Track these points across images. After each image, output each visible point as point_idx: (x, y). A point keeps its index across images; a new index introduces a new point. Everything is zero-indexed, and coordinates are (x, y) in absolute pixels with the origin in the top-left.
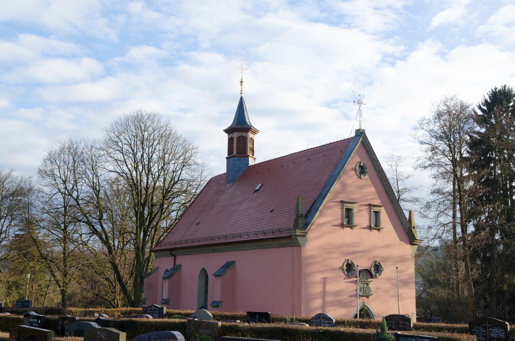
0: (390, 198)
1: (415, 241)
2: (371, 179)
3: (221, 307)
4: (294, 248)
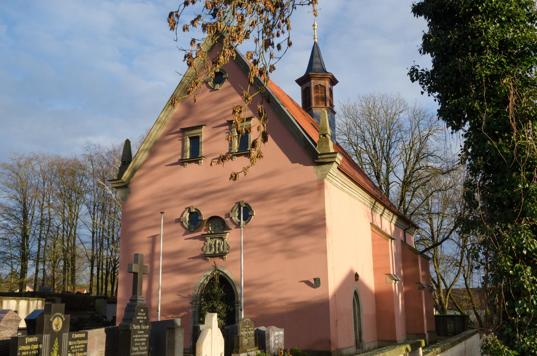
1: (319, 157)
2: (234, 85)
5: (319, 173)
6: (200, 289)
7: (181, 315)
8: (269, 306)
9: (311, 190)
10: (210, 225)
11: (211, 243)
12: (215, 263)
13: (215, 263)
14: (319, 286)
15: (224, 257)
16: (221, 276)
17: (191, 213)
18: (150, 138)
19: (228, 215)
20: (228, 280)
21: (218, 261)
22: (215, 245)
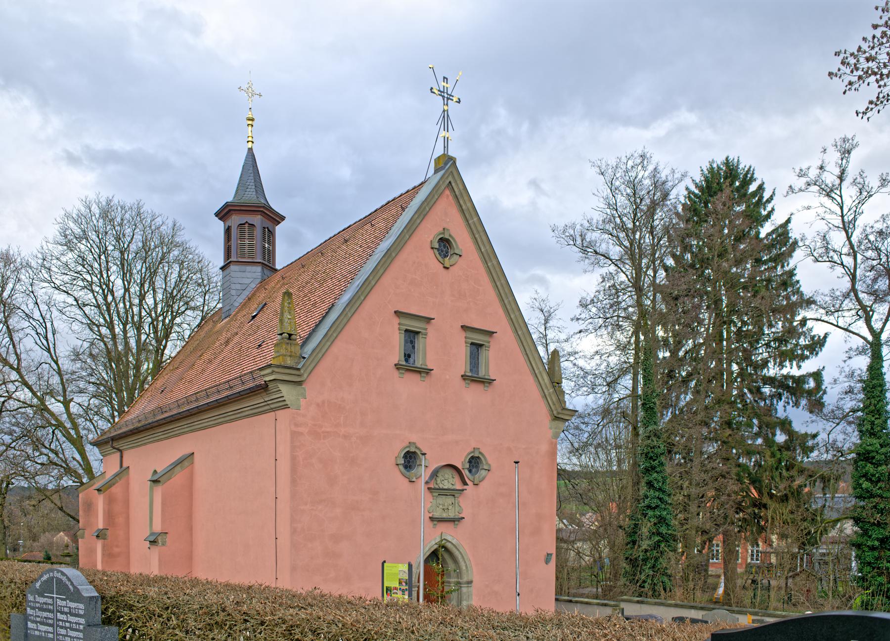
3: (163, 545)
4: (276, 412)
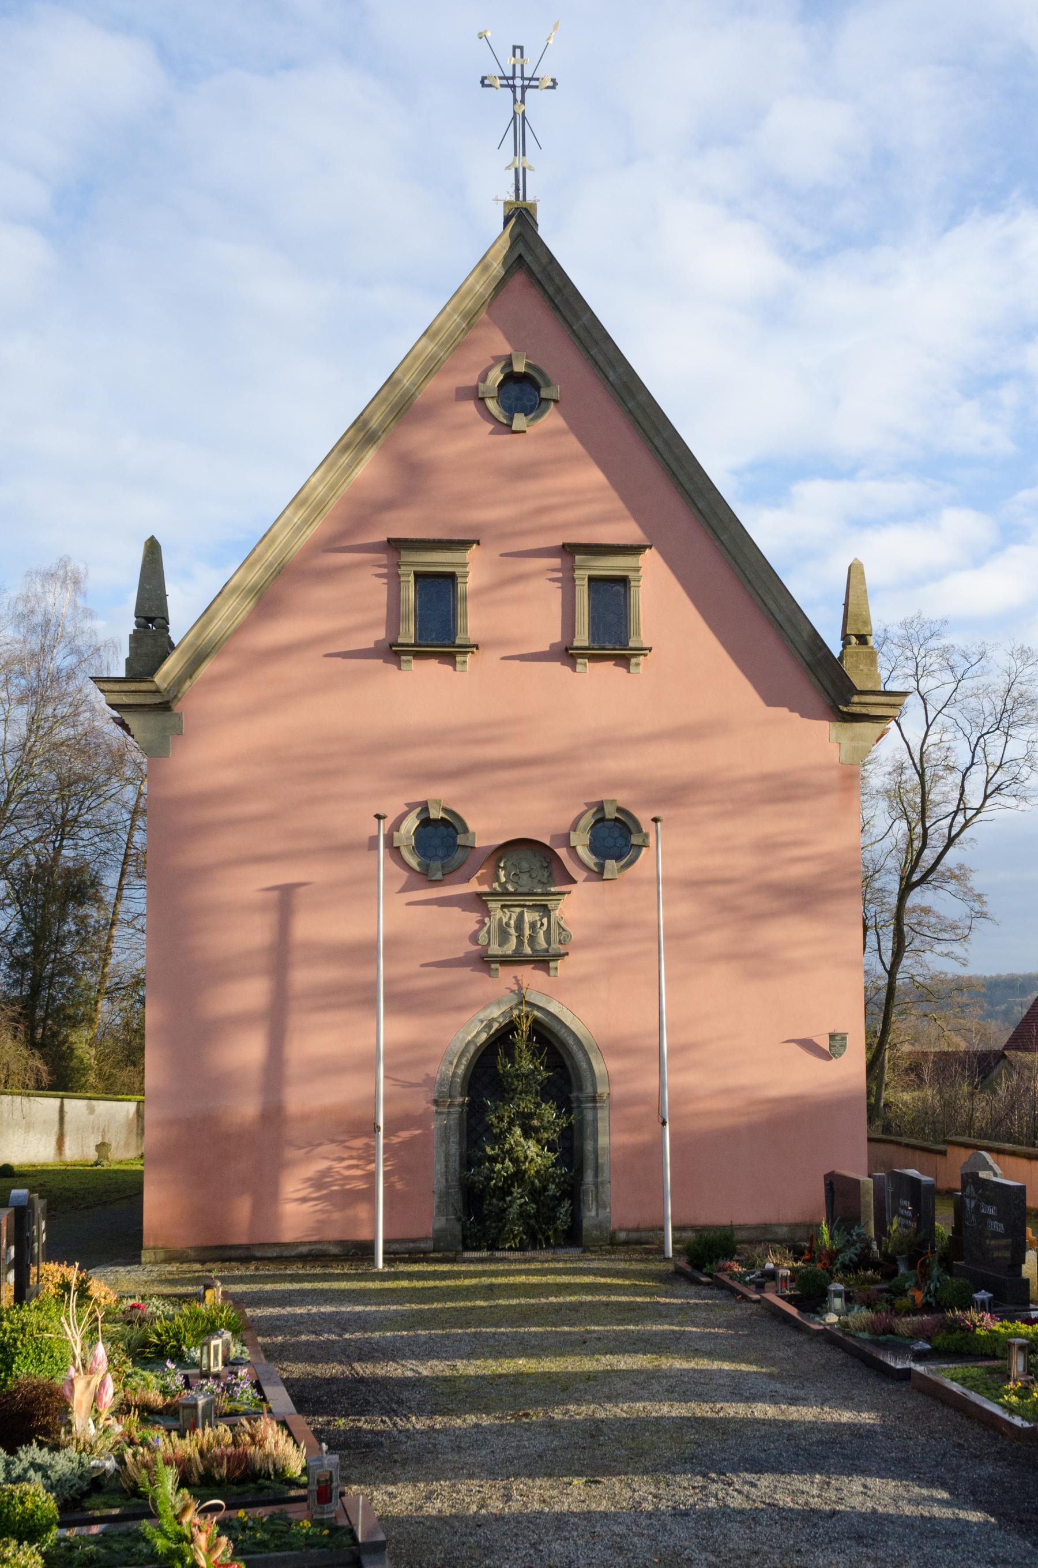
0: (699, 510)
1: (856, 699)
2: (577, 427)
5: (846, 743)
6: (465, 1059)
7: (400, 1140)
8: (692, 1108)
9: (821, 791)
10: (502, 865)
11: (505, 920)
12: (517, 982)
13: (517, 982)
14: (840, 1055)
15: (552, 965)
16: (536, 1021)
17: (426, 822)
18: (267, 551)
19: (565, 840)
20: (562, 1033)
21: (529, 975)
22: (519, 927)
